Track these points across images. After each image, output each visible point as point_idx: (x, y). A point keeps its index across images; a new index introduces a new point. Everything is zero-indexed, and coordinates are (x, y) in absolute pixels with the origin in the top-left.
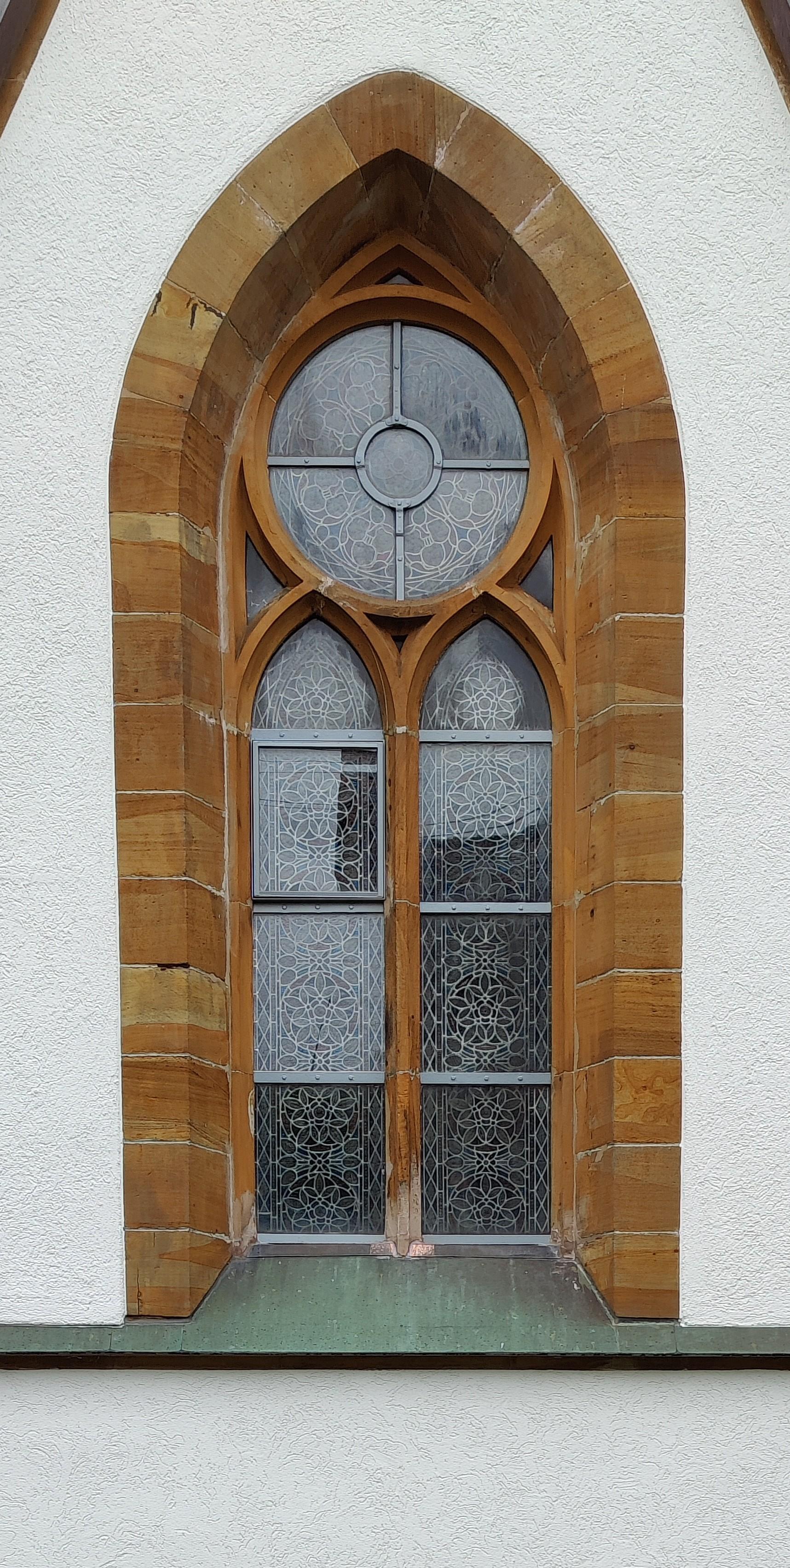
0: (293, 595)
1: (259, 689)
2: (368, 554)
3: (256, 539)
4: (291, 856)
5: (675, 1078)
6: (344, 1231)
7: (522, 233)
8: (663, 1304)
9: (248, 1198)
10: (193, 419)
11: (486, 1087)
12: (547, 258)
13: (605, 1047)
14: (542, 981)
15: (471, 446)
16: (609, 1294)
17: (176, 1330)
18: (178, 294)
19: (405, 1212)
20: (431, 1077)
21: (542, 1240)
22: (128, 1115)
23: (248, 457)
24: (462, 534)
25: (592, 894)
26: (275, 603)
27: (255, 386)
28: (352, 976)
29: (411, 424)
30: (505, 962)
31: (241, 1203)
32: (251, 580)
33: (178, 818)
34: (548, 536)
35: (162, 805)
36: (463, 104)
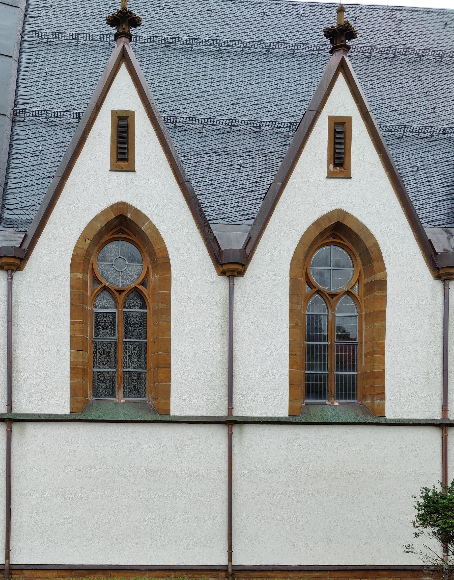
0: (101, 286)
1: (95, 302)
2: (114, 279)
3: (95, 277)
4: (100, 331)
5: (170, 372)
6: (108, 397)
7: (143, 228)
8: (167, 411)
9: (91, 391)
10: (85, 257)
11: (135, 372)
12: (147, 232)
13: (157, 366)
14: (145, 353)
15: (133, 261)
16: (158, 410)
17: (79, 415)
18: (83, 237)
19: (120, 394)
20: (125, 370)
21: (145, 399)
22: (71, 377)
23: (94, 263)
24: (131, 276)
25: (155, 339)
26: (98, 287)
27: (95, 251)
28: (110, 352)
29: (122, 257)
30: (138, 350)
31: (90, 392)
32: (94, 283)
33: (81, 325)
34: (146, 277)
35: (79, 323)
36: (133, 207)
